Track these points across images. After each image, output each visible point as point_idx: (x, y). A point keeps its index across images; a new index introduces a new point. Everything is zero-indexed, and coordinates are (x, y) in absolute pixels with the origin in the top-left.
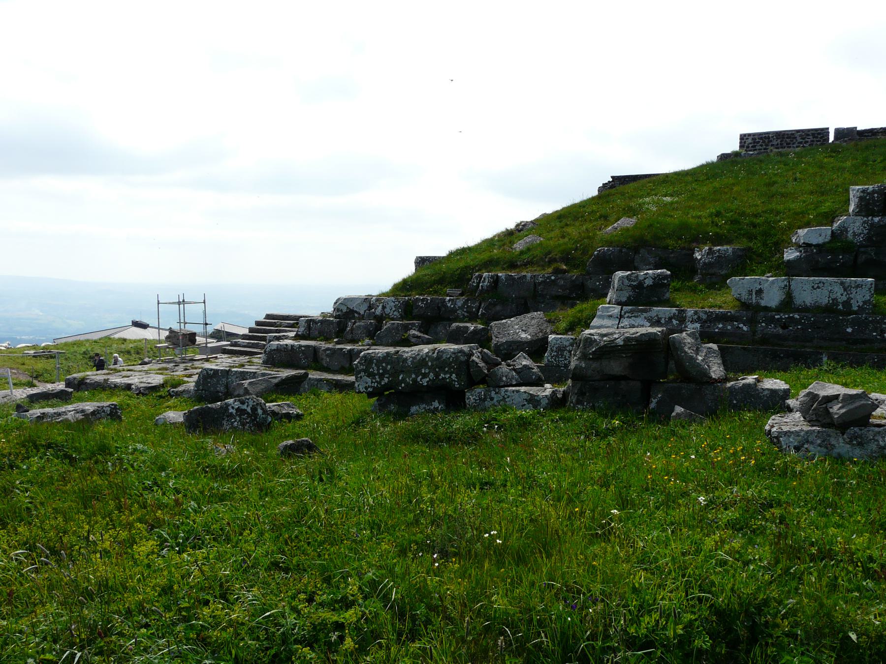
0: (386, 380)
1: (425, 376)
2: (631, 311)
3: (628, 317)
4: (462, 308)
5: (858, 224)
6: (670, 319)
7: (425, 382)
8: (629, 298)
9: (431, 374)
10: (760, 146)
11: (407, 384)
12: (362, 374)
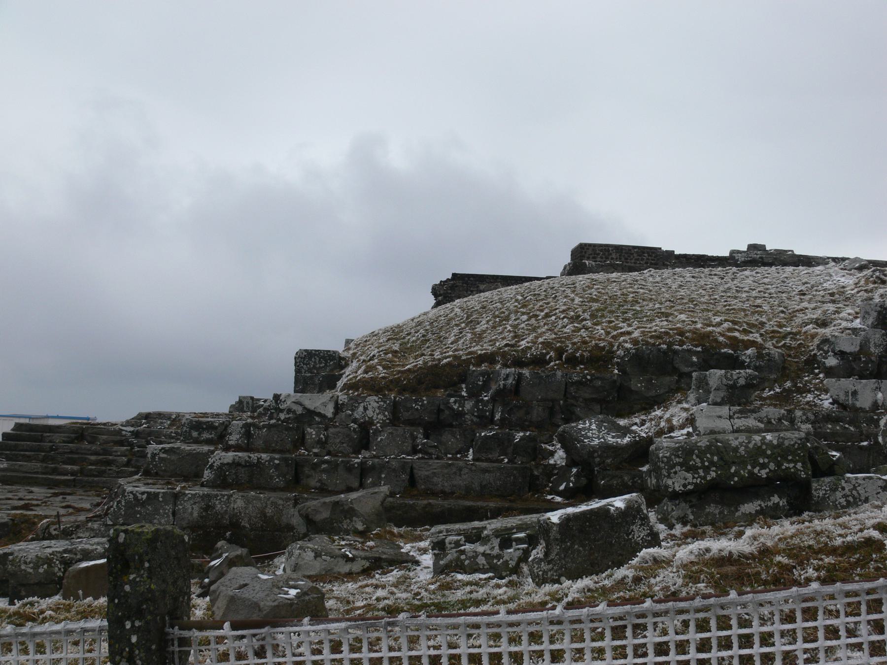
0: (713, 474)
1: (763, 466)
2: (740, 412)
3: (738, 418)
4: (471, 412)
5: (877, 336)
6: (780, 420)
7: (764, 473)
8: (723, 399)
9: (772, 464)
10: (455, 275)
11: (742, 478)
12: (678, 468)
